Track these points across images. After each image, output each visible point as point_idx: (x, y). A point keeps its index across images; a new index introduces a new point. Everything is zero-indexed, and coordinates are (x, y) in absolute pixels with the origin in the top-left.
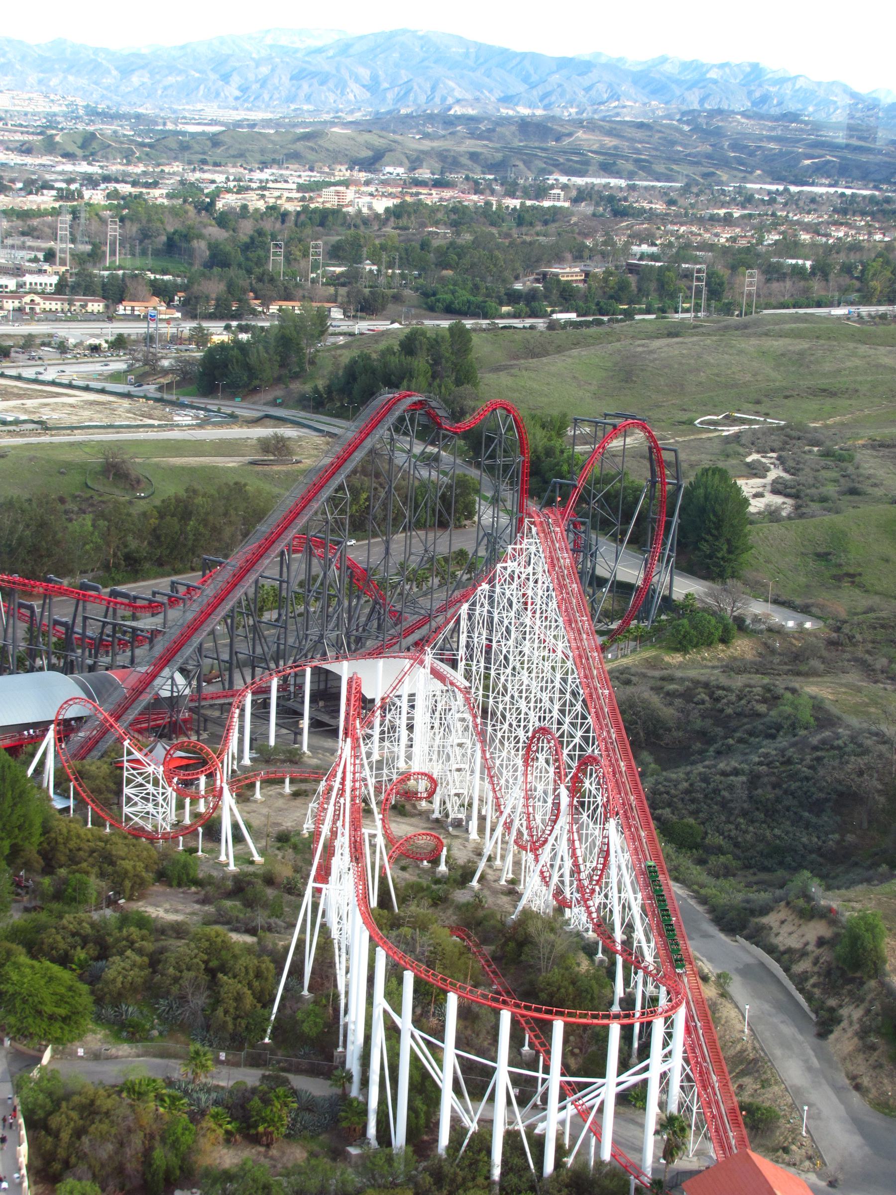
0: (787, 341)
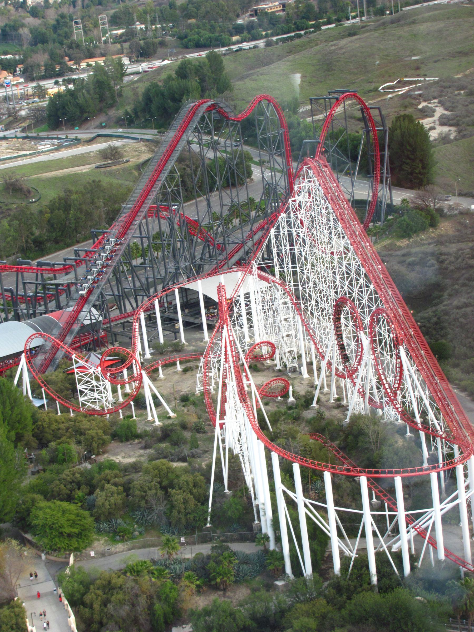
0: (429, 24)
